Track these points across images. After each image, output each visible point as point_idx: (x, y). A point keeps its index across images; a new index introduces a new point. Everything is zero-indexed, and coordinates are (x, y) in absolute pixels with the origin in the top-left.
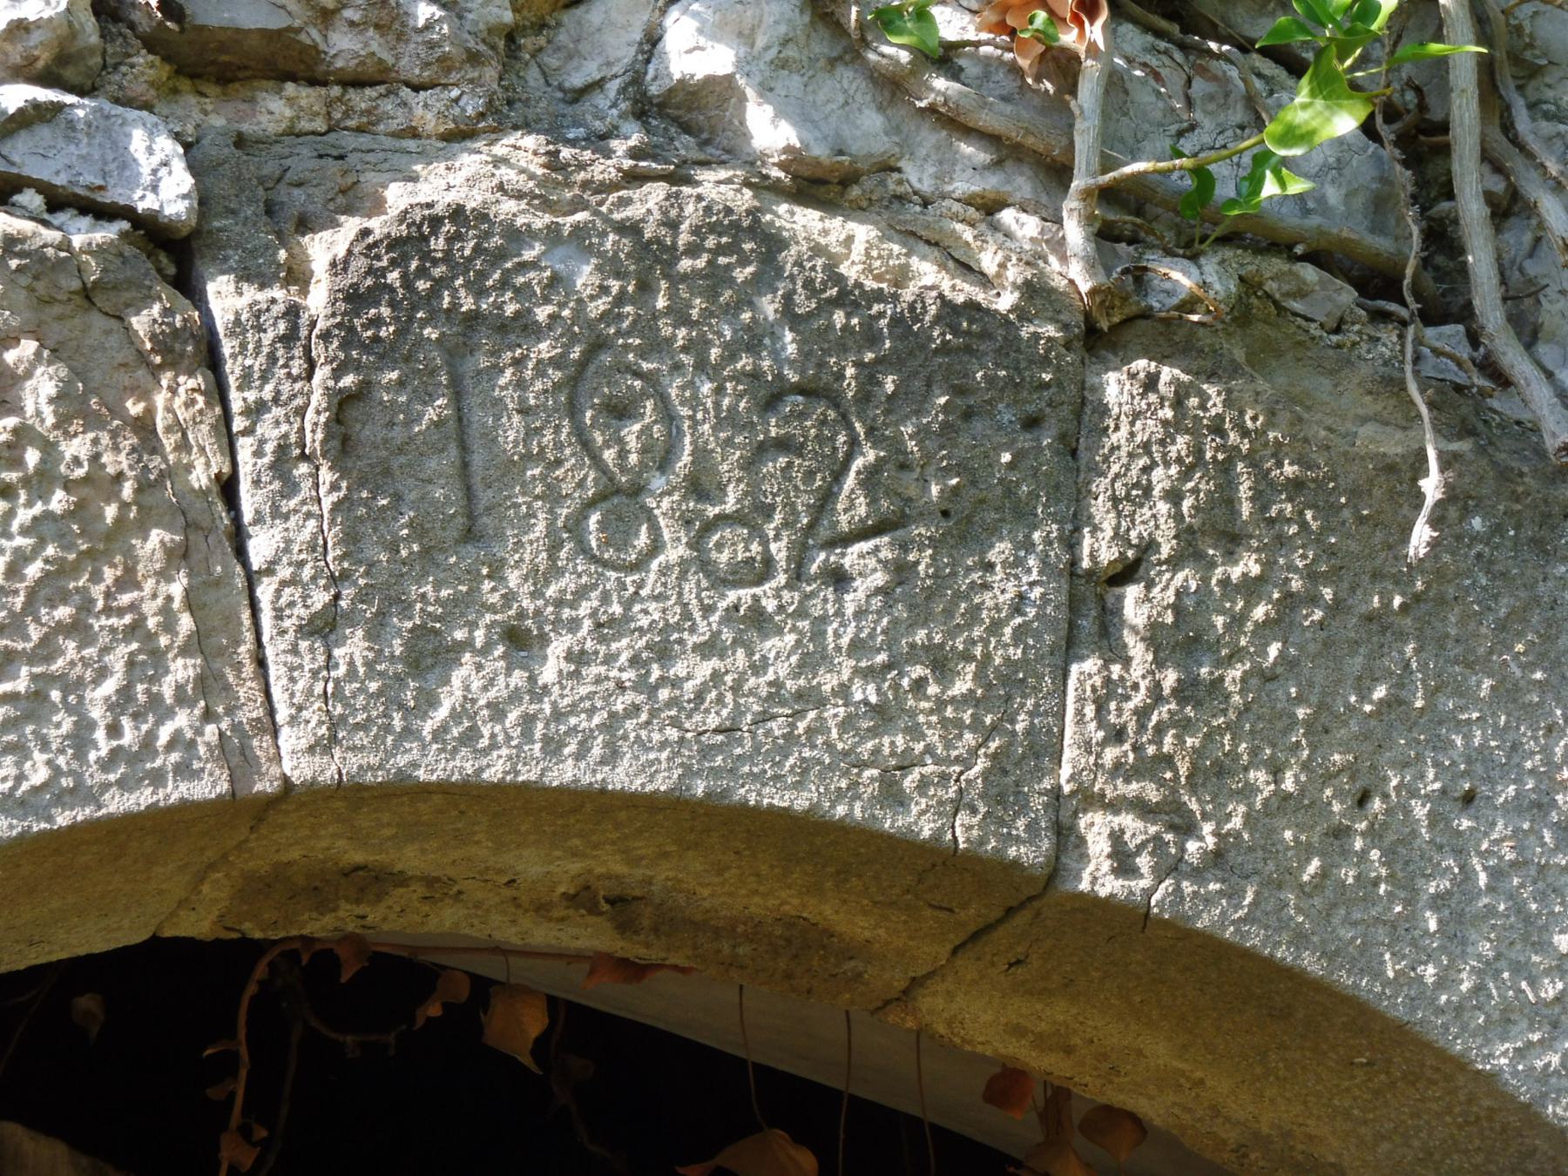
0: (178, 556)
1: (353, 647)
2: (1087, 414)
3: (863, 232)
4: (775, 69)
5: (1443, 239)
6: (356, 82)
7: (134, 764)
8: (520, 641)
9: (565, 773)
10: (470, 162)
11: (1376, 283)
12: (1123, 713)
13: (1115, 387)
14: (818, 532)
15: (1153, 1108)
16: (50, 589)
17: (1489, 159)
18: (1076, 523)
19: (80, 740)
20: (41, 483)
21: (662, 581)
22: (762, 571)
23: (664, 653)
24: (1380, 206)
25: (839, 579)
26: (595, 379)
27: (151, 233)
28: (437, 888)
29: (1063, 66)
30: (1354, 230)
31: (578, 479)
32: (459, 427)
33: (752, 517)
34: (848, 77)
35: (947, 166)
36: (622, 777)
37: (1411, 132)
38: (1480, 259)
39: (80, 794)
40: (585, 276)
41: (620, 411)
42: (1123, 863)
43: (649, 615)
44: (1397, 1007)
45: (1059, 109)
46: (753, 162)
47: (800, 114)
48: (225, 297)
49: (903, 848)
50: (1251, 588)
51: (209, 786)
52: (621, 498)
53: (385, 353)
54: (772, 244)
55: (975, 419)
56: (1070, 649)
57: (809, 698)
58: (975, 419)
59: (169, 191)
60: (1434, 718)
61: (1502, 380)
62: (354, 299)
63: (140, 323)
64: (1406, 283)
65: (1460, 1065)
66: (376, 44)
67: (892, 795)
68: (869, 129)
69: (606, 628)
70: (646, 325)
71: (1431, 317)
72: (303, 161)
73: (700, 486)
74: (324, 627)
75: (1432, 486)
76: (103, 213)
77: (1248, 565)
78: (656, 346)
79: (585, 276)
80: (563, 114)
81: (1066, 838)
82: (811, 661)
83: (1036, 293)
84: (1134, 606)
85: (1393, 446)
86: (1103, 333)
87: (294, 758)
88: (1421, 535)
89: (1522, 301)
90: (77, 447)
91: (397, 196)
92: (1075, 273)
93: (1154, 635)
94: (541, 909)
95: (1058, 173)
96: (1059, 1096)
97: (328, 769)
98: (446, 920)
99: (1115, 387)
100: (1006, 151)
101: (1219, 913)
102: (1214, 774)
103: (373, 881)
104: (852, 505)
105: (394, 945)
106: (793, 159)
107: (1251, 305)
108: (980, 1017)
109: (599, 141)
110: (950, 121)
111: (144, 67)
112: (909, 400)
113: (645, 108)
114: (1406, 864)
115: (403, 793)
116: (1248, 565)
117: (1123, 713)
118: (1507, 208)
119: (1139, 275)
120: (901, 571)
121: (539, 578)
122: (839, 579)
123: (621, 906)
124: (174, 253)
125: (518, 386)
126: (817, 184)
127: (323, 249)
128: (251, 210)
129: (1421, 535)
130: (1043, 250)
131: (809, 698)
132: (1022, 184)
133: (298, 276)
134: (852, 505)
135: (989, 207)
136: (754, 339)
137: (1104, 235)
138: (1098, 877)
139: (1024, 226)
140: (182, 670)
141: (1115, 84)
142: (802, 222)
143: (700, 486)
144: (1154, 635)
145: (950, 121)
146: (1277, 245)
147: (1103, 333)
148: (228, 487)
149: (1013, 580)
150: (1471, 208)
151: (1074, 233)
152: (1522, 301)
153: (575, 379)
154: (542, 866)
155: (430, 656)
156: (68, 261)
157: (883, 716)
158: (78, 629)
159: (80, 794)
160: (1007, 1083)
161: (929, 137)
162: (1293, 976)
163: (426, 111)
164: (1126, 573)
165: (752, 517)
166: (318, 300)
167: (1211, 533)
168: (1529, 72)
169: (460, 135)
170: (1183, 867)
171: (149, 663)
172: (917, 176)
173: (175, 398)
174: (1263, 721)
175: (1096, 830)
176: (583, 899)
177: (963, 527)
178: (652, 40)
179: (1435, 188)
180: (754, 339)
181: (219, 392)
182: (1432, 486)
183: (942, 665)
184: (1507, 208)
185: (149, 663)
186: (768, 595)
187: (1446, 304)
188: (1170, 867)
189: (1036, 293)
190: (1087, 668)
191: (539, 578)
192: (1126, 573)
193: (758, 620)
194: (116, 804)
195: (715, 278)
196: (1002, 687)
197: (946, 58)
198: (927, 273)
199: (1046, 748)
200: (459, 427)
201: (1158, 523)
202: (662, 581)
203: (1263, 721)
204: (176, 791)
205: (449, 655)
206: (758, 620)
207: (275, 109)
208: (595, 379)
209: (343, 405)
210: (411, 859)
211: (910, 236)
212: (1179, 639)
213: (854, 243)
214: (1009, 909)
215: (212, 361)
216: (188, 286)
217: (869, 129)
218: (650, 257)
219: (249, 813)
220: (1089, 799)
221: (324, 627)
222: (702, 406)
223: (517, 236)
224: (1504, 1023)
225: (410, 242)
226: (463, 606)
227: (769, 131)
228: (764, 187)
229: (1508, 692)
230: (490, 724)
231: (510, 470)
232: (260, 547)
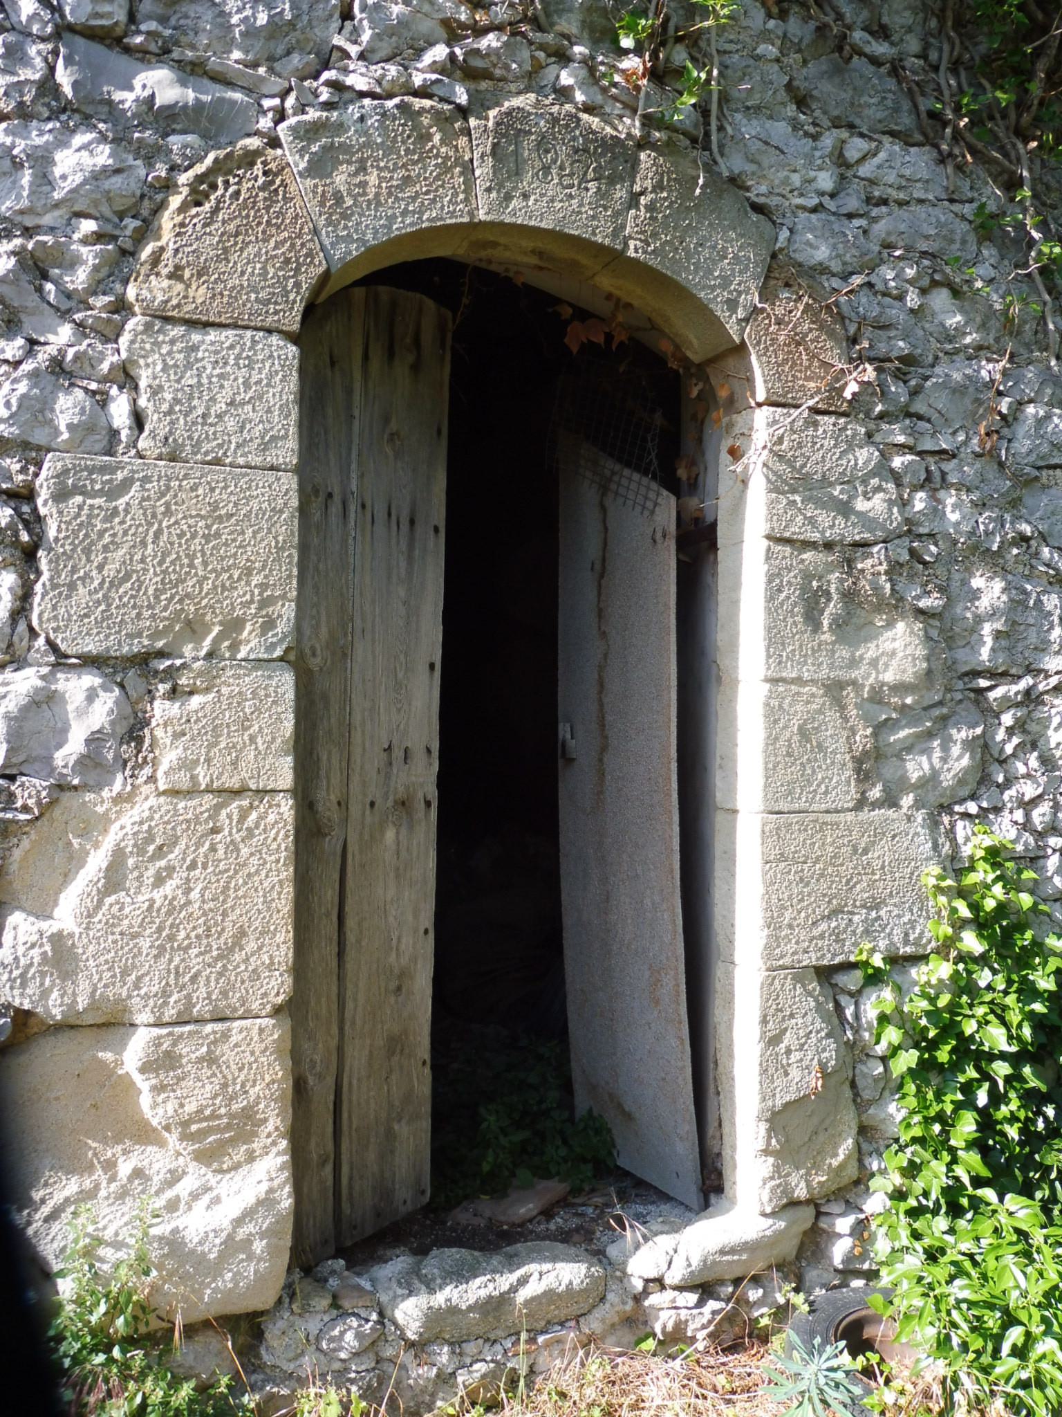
0: (462, 173)
1: (494, 195)
2: (636, 162)
3: (597, 120)
4: (582, 84)
5: (707, 134)
6: (500, 80)
7: (452, 214)
8: (526, 196)
9: (532, 223)
10: (521, 98)
11: (694, 140)
12: (639, 221)
13: (643, 156)
14: (583, 180)
15: (635, 303)
16: (437, 178)
17: (718, 119)
18: (633, 182)
19: (442, 208)
20: (437, 156)
21: (552, 189)
22: (572, 186)
23: (552, 201)
24: (696, 126)
25: (587, 189)
26: (543, 144)
27: (459, 107)
28: (506, 247)
29: (638, 88)
30: (691, 129)
31: (538, 164)
32: (516, 152)
33: (571, 175)
34: (596, 88)
35: (614, 107)
36: (543, 225)
37: (702, 109)
38: (714, 138)
39: (442, 219)
40: (542, 123)
41: (547, 151)
42: (636, 251)
43: (550, 193)
44: (684, 283)
45: (637, 98)
46: (576, 104)
47: (586, 94)
48: (473, 122)
49: (595, 243)
50: (665, 199)
51: (466, 220)
52: (546, 169)
53: (503, 135)
54: (579, 120)
55: (615, 160)
56: (630, 208)
57: (580, 213)
58: (615, 160)
59: (462, 97)
60: (697, 229)
61: (716, 162)
62: (498, 124)
63: (457, 125)
64: (700, 141)
65: (694, 296)
66: (503, 72)
67: (594, 234)
68: (599, 99)
69: (542, 195)
70: (553, 134)
71: (704, 149)
72: (489, 96)
73: (562, 168)
74: (489, 190)
75: (701, 182)
76: (450, 103)
77: (665, 194)
78: (555, 138)
79: (542, 123)
80: (540, 90)
81: (626, 245)
82: (581, 205)
83: (629, 135)
84: (643, 200)
85: (694, 173)
86: (642, 144)
87: (482, 215)
88: (698, 191)
89: (721, 147)
90: (443, 150)
91: (507, 104)
92: (637, 132)
93: (646, 206)
94: (525, 253)
95: (635, 111)
96: (619, 300)
97: (489, 218)
98: (507, 254)
99: (643, 156)
100: (626, 105)
101: (653, 262)
102: (655, 235)
103: (495, 245)
104: (591, 175)
105: (431, 688)
106: (584, 103)
107: (669, 143)
108: (606, 282)
109: (546, 97)
110: (615, 98)
111: (458, 73)
112: (603, 155)
113: (555, 91)
114: (689, 256)
115: (502, 224)
116: (665, 194)
117: (639, 221)
118: (721, 129)
119: (649, 134)
120: (599, 189)
121: (530, 184)
122: (587, 189)
123: (541, 254)
124: (463, 112)
125: (529, 143)
126: (588, 109)
127: (492, 113)
128: (478, 105)
129: (698, 191)
130: (630, 127)
131: (580, 213)
132: (628, 112)
133: (487, 119)
134: (591, 175)
135: (621, 117)
136: (574, 139)
137: (643, 125)
138: (631, 253)
139: (627, 121)
140: (462, 196)
141: (647, 93)
142: (585, 117)
143: (562, 168)
144: (646, 206)
145: (615, 98)
146: (676, 131)
147: (642, 144)
148: (471, 160)
149: (620, 193)
150: (714, 127)
151: (637, 123)
152: (721, 147)
153: (539, 144)
154: (528, 244)
155: (508, 198)
156: (443, 112)
157: (594, 217)
158: (442, 186)
159: (442, 219)
160: (609, 297)
161: (610, 101)
162: (665, 276)
163: (513, 87)
164: (642, 193)
165: (571, 175)
166: (490, 124)
167: (658, 187)
168: (728, 101)
169: (519, 93)
170: (573, 1324)
171: (455, 194)
172: (608, 109)
173: (462, 141)
174: (665, 225)
175: (632, 243)
176: (533, 252)
177: (612, 181)
178: (558, 77)
179: (707, 124)
180: (574, 139)
181: (471, 141)
182: (701, 182)
183: (605, 208)
184: (721, 129)
185: (455, 194)
186: (573, 191)
187: (707, 147)
188: (645, 252)
189: (629, 135)
190: (633, 212)
191: (530, 184)
192: (642, 193)
193: (571, 196)
194: (449, 221)
195: (567, 126)
196: (617, 214)
197: (615, 85)
198: (608, 130)
199: (623, 227)
200: (516, 152)
201: (648, 184)
202: (552, 189)
203: (665, 225)
204: (460, 220)
205: (512, 198)
206: (571, 196)
207: (484, 85)
208: (543, 144)
209: (494, 145)
210: (502, 240)
211: (606, 122)
212: (650, 208)
213: (594, 122)
214: (613, 258)
215: (470, 135)
216: (466, 119)
217: (599, 99)
218: (555, 120)
219: (475, 226)
220: (631, 238)
221: (489, 190)
222: (563, 150)
223: (530, 114)
224: (703, 288)
225: (509, 113)
226: (515, 188)
227: (580, 97)
228: (578, 109)
229: (710, 225)
230: (519, 212)
231: (525, 161)
232: (477, 173)
